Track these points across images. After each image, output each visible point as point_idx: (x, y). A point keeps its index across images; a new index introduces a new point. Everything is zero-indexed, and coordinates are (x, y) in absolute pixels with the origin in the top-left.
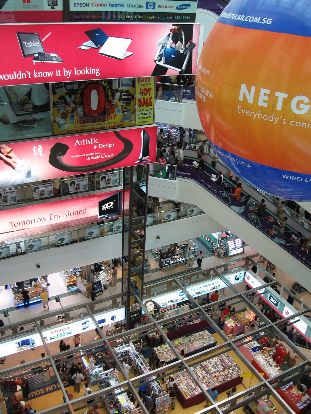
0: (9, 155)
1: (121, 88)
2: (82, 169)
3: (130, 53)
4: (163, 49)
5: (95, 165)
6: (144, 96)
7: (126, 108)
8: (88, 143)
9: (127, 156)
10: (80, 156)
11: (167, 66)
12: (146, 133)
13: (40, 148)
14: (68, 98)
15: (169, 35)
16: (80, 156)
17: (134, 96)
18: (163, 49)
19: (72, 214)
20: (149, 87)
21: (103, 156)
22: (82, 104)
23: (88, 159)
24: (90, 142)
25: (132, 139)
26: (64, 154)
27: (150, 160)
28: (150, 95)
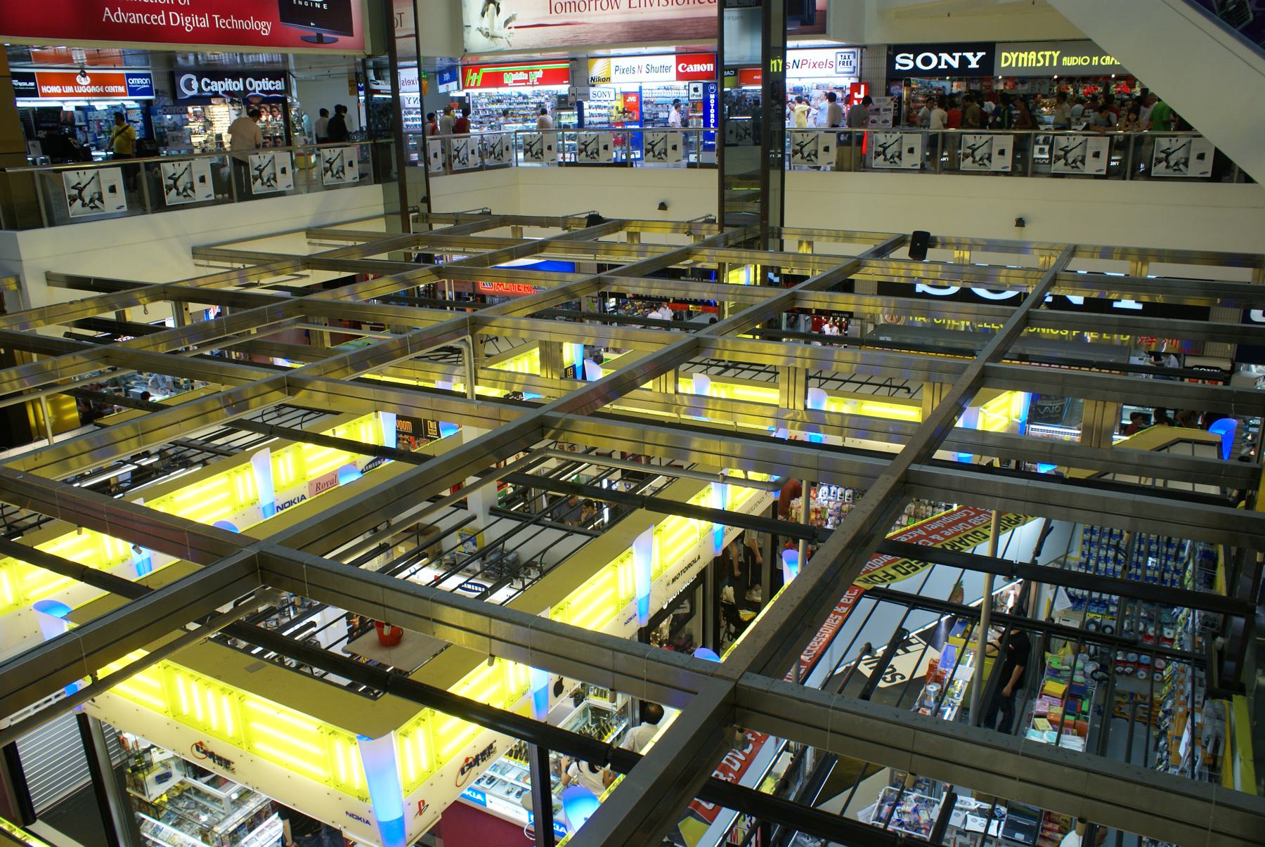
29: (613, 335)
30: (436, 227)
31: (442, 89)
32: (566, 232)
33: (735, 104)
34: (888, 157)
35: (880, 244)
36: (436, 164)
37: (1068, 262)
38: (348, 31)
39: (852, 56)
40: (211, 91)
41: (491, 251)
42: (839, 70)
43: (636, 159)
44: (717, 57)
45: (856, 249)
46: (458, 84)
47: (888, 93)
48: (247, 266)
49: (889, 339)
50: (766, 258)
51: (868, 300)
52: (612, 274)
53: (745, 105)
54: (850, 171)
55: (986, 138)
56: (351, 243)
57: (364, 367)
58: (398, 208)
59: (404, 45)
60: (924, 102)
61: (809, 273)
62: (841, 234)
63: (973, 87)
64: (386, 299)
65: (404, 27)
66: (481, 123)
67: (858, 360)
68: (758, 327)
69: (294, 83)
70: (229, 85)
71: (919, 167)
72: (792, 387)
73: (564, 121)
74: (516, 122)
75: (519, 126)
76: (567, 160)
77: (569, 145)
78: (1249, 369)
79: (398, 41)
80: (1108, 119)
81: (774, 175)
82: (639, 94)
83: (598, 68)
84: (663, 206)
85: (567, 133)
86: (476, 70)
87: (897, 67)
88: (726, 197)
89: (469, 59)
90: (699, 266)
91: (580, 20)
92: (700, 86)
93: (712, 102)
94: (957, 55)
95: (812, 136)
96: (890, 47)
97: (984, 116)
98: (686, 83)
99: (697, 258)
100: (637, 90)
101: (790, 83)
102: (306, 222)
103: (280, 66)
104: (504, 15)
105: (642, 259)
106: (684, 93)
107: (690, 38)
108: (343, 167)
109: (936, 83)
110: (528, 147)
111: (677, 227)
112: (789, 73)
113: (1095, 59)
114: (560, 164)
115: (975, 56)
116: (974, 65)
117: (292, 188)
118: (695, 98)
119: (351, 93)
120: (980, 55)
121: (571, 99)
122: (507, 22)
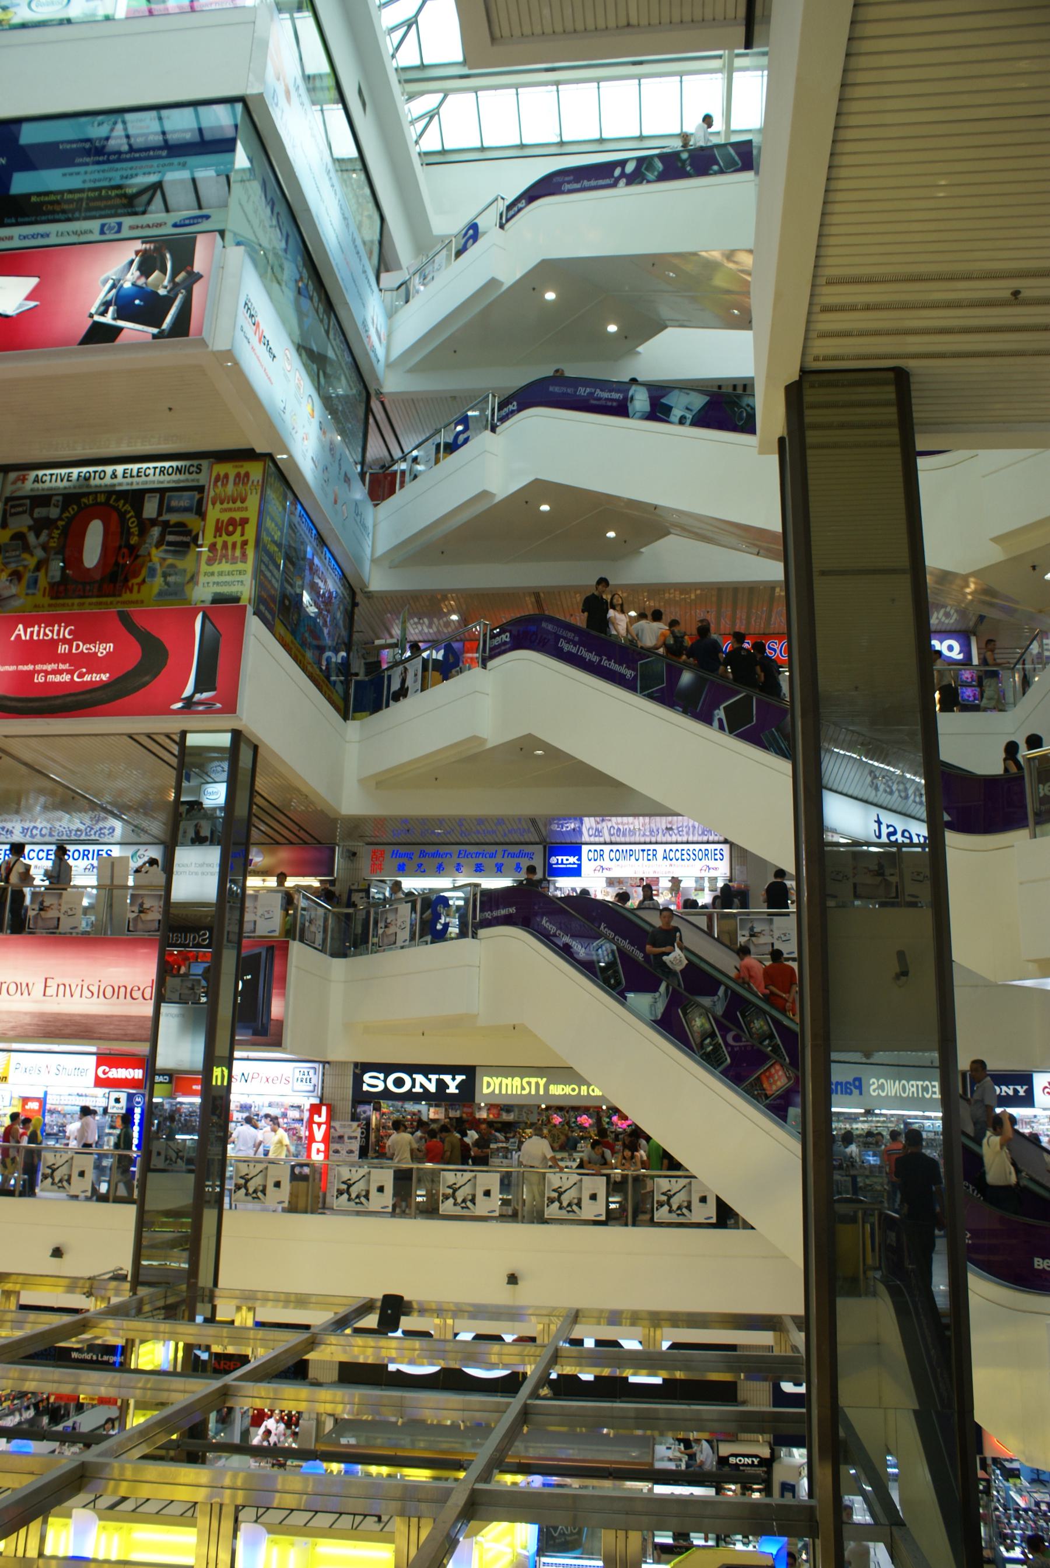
1: (165, 517)
2: (19, 705)
4: (114, 291)
5: (56, 698)
6: (225, 537)
7: (172, 566)
8: (45, 634)
9: (148, 683)
10: (21, 668)
11: (121, 323)
14: (31, 538)
15: (132, 262)
16: (21, 668)
17: (197, 535)
18: (114, 291)
20: (243, 515)
21: (78, 677)
22: (60, 551)
23: (39, 679)
24: (50, 634)
25: (165, 635)
27: (219, 705)
28: (242, 535)
35: (342, 1311)
37: (571, 1330)
39: (312, 1072)
42: (296, 1088)
44: (148, 1063)
45: (317, 1318)
47: (355, 1117)
49: (374, 1470)
50: (193, 1331)
51: (324, 1394)
53: (180, 1120)
54: (306, 1212)
55: (468, 1175)
61: (249, 1352)
62: (293, 1298)
63: (452, 1114)
67: (310, 1489)
68: (174, 1437)
71: (390, 1209)
72: (214, 1539)
78: (791, 1455)
80: (603, 1156)
81: (209, 1216)
82: (42, 1102)
84: (57, 1253)
87: (365, 1088)
90: (99, 1342)
92: (123, 1097)
93: (137, 1118)
94: (434, 1077)
95: (260, 1167)
97: (465, 1147)
98: (107, 1090)
100: (42, 1095)
101: (236, 1098)
105: (19, 1334)
109: (411, 1107)
111: (73, 1284)
112: (235, 1087)
113: (584, 1088)
115: (454, 1079)
116: (452, 1089)
118: (115, 1111)
120: (460, 1078)
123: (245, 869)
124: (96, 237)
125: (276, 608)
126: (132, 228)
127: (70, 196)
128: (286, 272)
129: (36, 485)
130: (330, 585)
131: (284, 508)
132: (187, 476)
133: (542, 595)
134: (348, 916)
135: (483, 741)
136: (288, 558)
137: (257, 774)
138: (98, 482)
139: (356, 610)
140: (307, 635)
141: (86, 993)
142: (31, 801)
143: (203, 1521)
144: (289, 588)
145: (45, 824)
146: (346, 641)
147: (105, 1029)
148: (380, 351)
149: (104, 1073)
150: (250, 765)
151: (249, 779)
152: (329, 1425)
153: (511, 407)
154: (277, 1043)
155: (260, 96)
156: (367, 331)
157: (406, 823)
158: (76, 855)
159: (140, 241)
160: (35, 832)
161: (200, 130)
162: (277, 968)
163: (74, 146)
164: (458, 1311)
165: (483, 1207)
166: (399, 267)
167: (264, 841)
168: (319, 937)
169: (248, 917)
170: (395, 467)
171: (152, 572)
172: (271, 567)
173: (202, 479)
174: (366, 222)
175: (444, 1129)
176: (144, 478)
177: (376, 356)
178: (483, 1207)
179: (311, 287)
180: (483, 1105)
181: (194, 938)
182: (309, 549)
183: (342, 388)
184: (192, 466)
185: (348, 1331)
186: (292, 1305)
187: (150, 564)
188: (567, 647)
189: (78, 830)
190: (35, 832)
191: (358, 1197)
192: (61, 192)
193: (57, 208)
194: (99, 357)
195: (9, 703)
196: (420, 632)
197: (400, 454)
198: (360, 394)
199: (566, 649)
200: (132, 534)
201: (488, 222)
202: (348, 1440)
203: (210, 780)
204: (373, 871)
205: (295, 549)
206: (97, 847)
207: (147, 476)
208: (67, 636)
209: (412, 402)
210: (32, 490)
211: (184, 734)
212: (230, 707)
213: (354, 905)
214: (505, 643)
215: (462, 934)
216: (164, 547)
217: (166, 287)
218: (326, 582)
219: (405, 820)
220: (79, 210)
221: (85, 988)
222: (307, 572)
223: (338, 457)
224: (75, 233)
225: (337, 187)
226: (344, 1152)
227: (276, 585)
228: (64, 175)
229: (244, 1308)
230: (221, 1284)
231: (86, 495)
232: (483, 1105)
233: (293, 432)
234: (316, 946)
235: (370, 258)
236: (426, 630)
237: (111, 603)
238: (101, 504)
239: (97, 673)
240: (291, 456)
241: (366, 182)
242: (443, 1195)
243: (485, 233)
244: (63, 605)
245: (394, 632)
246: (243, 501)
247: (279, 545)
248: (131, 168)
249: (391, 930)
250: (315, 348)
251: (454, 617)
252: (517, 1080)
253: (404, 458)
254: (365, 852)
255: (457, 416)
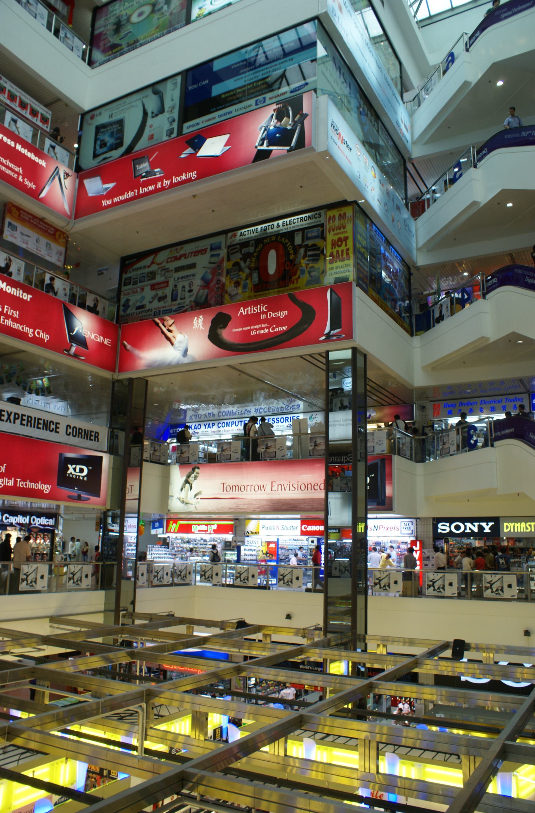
0: (171, 328)
1: (306, 243)
3: (228, 148)
4: (266, 132)
6: (337, 248)
7: (312, 267)
8: (254, 311)
10: (244, 329)
12: (335, 292)
13: (201, 319)
14: (242, 264)
16: (244, 329)
17: (323, 250)
18: (266, 132)
19: (303, 487)
20: (345, 235)
21: (272, 330)
22: (257, 268)
23: (253, 333)
25: (313, 303)
26: (225, 327)
27: (343, 335)
28: (346, 245)
29: (247, 711)
30: (138, 622)
31: (153, 532)
32: (222, 631)
33: (338, 551)
34: (436, 588)
35: (432, 647)
36: (142, 580)
38: (98, 494)
39: (410, 524)
40: (8, 522)
41: (171, 642)
42: (402, 532)
43: (272, 584)
44: (324, 522)
45: (418, 651)
46: (163, 530)
48: (5, 639)
49: (455, 731)
50: (357, 656)
51: (427, 690)
52: (249, 664)
53: (345, 551)
54: (411, 596)
55: (498, 576)
56: (78, 629)
57: (72, 721)
58: (113, 607)
59: (131, 504)
60: (458, 552)
62: (407, 640)
63: (488, 544)
64: (96, 672)
65: (132, 494)
66: (175, 555)
69: (61, 521)
70: (20, 519)
71: (456, 595)
72: (367, 758)
73: (227, 558)
74: (198, 556)
75: (199, 559)
76: (228, 583)
77: (230, 573)
79: (127, 502)
81: (360, 599)
82: (277, 543)
83: (251, 526)
84: (289, 617)
85: (230, 565)
86: (175, 521)
87: (439, 531)
88: (330, 612)
89: (172, 515)
91: (240, 497)
92: (315, 540)
94: (476, 524)
96: (434, 519)
98: (307, 537)
99: (308, 654)
100: (276, 540)
102: (51, 611)
103: (54, 511)
104: (194, 491)
105: (274, 653)
106: (306, 543)
107: (309, 511)
108: (81, 578)
109: (465, 541)
110: (203, 573)
111: (298, 632)
112: (369, 533)
114: (223, 585)
115: (487, 525)
116: (487, 530)
117: (46, 588)
118: (312, 547)
119: (96, 530)
120: (491, 524)
121: (233, 544)
122: (196, 495)
123: (366, 420)
124: (254, 107)
125: (368, 282)
126: (270, 98)
127: (240, 90)
128: (352, 103)
129: (241, 237)
130: (396, 266)
131: (366, 228)
132: (314, 220)
133: (514, 254)
134: (423, 440)
135: (488, 339)
136: (371, 254)
137: (367, 369)
138: (271, 230)
139: (412, 277)
140: (386, 293)
141: (292, 488)
142: (258, 395)
143: (361, 749)
144: (374, 270)
145: (266, 406)
146: (408, 294)
147: (302, 506)
148: (408, 136)
149: (305, 528)
150: (363, 365)
151: (363, 373)
152: (431, 706)
153: (484, 152)
154: (390, 509)
155: (326, 13)
156: (399, 126)
157: (451, 388)
158: (282, 420)
159: (275, 104)
160: (261, 410)
161: (300, 39)
162: (387, 470)
163: (239, 65)
164: (498, 650)
165: (507, 593)
166: (413, 88)
167: (375, 404)
168: (408, 453)
169: (369, 444)
170: (424, 198)
171: (303, 272)
172: (363, 260)
173: (322, 220)
174: (392, 67)
175: (485, 551)
176: (293, 225)
177: (406, 139)
178: (507, 593)
179: (366, 109)
180: (505, 538)
181: (346, 459)
182: (382, 248)
183: (389, 161)
184: (316, 214)
185: (436, 658)
186: (407, 644)
187: (301, 268)
188: (530, 281)
189: (282, 407)
190: (261, 410)
191: (439, 588)
192: (235, 89)
193: (234, 98)
194: (263, 167)
195: (240, 347)
196: (448, 285)
197: (426, 190)
198: (400, 161)
199: (530, 282)
200: (291, 254)
201: (459, 50)
202: (440, 715)
203: (345, 376)
204: (435, 416)
205: (374, 249)
206: (292, 416)
207: (294, 223)
208: (265, 310)
209: (428, 160)
210: (240, 240)
211: (327, 352)
212: (349, 336)
213: (426, 434)
214: (495, 283)
215: (485, 445)
216: (307, 258)
217: (290, 125)
218: (393, 265)
219: (449, 387)
220: (244, 96)
221: (291, 486)
222: (383, 261)
223: (392, 197)
224: (244, 108)
225: (373, 52)
226: (430, 565)
227: (367, 269)
228: (236, 80)
229: (381, 645)
230: (369, 633)
231: (266, 238)
232: (505, 538)
233: (366, 187)
234: (407, 457)
235: (396, 86)
236: (451, 283)
237: (284, 290)
238: (274, 241)
239: (281, 327)
240: (366, 200)
241: (389, 46)
242: (485, 587)
243: (457, 58)
244: (261, 295)
245: (433, 287)
246: (344, 228)
247: (366, 248)
248: (267, 69)
249: (446, 446)
250: (372, 141)
251: (466, 274)
252: (523, 524)
253: (428, 192)
254: (430, 406)
255: (454, 163)
